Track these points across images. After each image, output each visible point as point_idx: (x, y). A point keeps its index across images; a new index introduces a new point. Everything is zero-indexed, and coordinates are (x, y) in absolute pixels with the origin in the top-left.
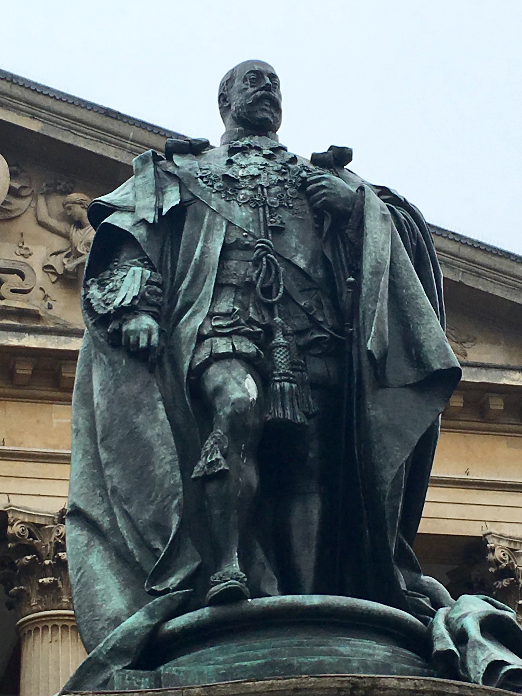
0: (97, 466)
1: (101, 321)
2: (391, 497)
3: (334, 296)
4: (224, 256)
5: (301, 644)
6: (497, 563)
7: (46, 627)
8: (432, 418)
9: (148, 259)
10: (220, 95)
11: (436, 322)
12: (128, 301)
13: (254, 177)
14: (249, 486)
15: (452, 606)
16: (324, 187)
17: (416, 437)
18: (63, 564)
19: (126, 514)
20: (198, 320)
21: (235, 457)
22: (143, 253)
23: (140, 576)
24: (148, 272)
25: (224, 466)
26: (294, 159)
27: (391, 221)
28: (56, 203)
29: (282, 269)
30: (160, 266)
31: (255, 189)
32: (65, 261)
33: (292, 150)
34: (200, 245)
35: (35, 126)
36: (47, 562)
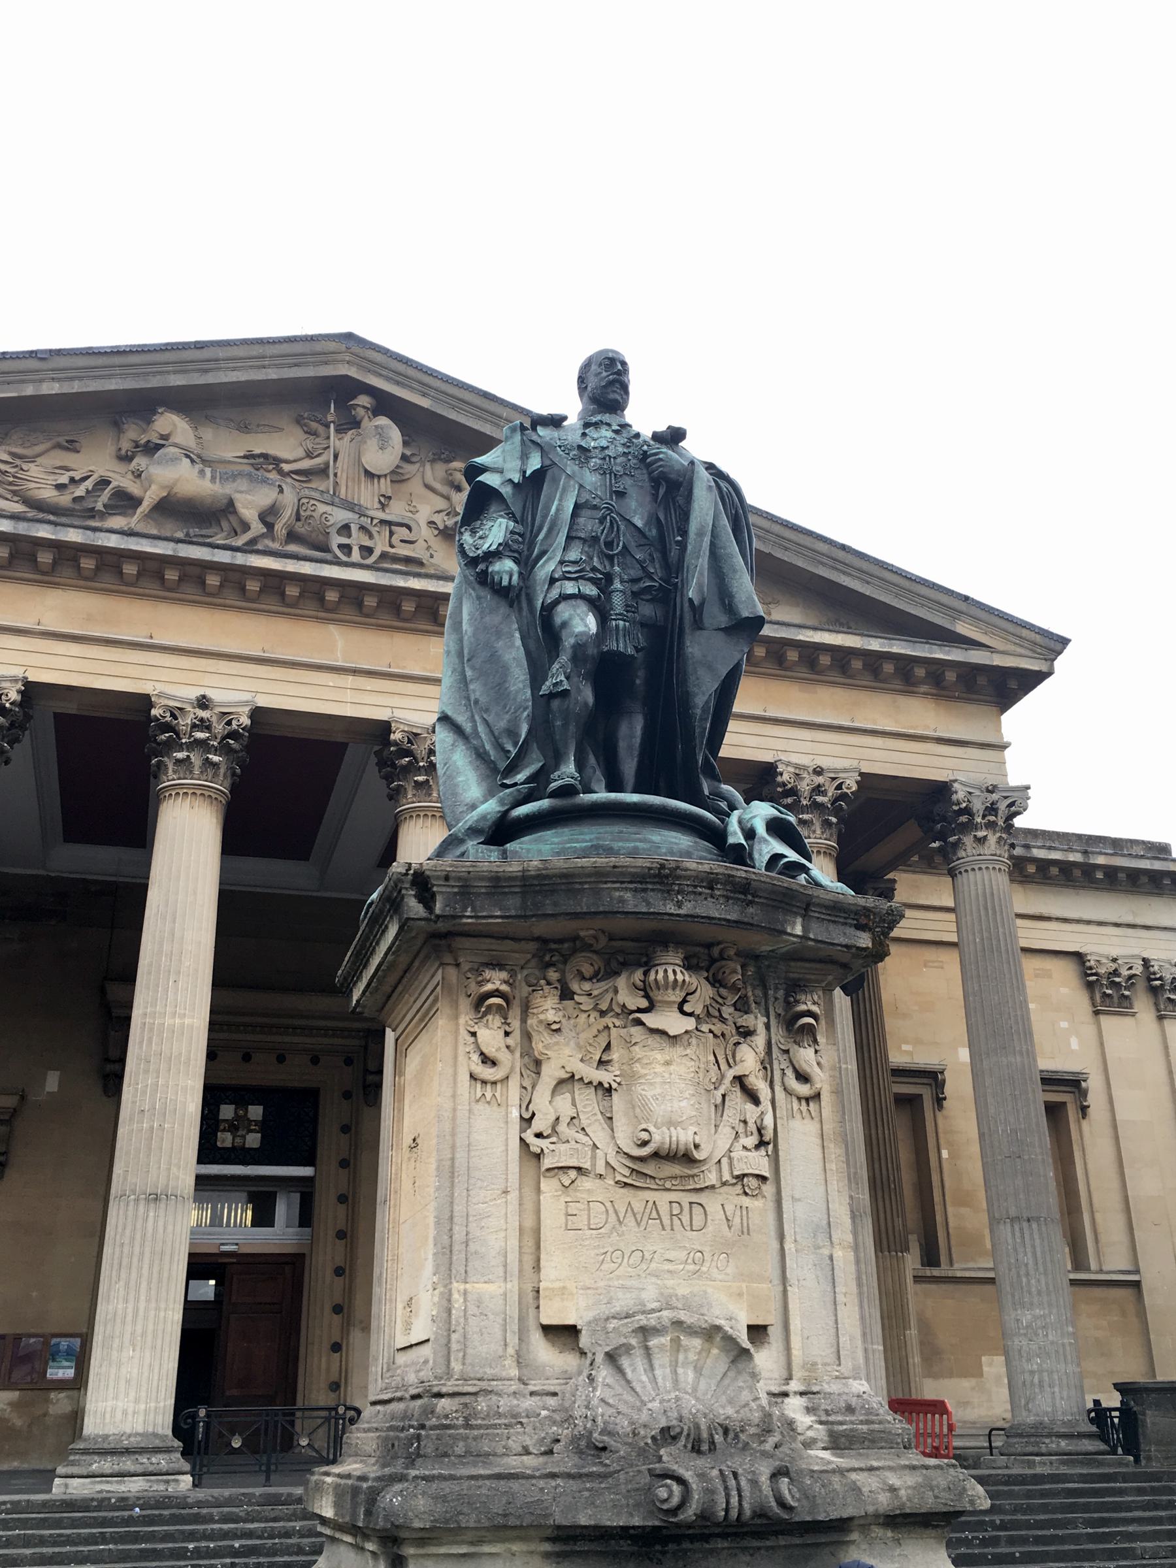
0: (463, 682)
1: (472, 562)
2: (701, 719)
3: (664, 553)
4: (574, 515)
5: (621, 832)
6: (784, 785)
7: (418, 816)
8: (738, 656)
9: (512, 513)
10: (580, 377)
11: (746, 578)
12: (494, 547)
13: (603, 448)
14: (586, 704)
15: (744, 809)
16: (661, 460)
17: (724, 672)
18: (432, 766)
19: (486, 722)
20: (551, 566)
21: (575, 679)
22: (508, 507)
23: (496, 772)
24: (512, 524)
25: (566, 686)
26: (637, 435)
27: (716, 492)
28: (440, 468)
29: (622, 527)
30: (522, 520)
31: (604, 459)
32: (446, 518)
33: (636, 428)
34: (556, 503)
35: (425, 403)
36: (421, 764)
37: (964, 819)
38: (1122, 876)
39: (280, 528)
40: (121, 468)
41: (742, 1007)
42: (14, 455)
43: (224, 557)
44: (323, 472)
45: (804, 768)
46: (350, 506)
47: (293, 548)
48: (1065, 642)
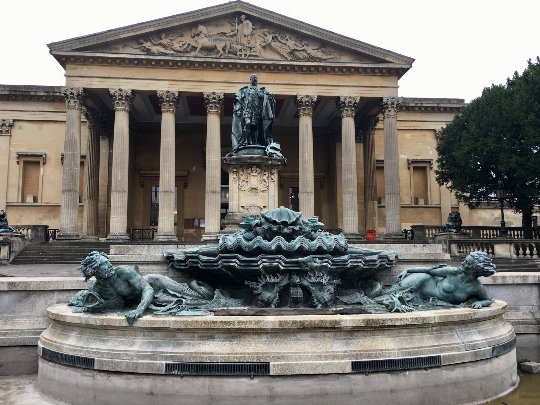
28: (262, 30)
35: (257, 15)
37: (386, 106)
38: (448, 109)
39: (227, 51)
40: (192, 39)
41: (265, 171)
42: (170, 40)
43: (215, 60)
44: (235, 35)
45: (347, 97)
46: (241, 44)
47: (230, 55)
48: (414, 60)
